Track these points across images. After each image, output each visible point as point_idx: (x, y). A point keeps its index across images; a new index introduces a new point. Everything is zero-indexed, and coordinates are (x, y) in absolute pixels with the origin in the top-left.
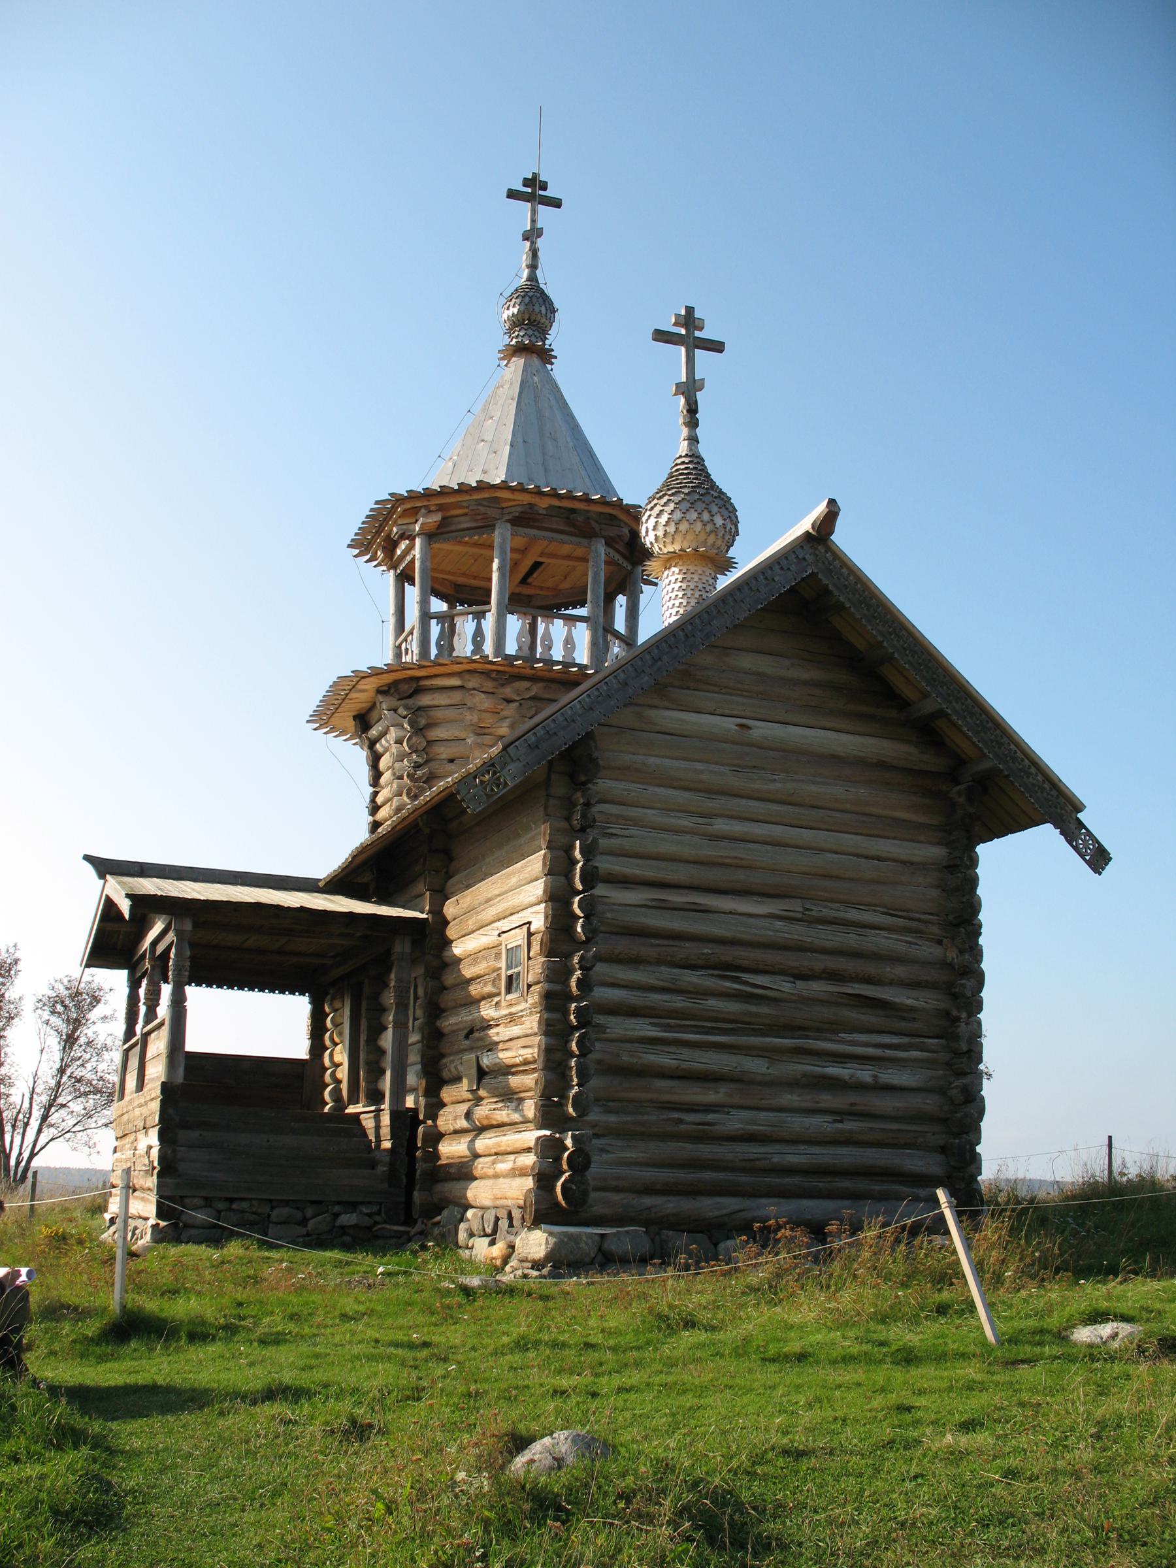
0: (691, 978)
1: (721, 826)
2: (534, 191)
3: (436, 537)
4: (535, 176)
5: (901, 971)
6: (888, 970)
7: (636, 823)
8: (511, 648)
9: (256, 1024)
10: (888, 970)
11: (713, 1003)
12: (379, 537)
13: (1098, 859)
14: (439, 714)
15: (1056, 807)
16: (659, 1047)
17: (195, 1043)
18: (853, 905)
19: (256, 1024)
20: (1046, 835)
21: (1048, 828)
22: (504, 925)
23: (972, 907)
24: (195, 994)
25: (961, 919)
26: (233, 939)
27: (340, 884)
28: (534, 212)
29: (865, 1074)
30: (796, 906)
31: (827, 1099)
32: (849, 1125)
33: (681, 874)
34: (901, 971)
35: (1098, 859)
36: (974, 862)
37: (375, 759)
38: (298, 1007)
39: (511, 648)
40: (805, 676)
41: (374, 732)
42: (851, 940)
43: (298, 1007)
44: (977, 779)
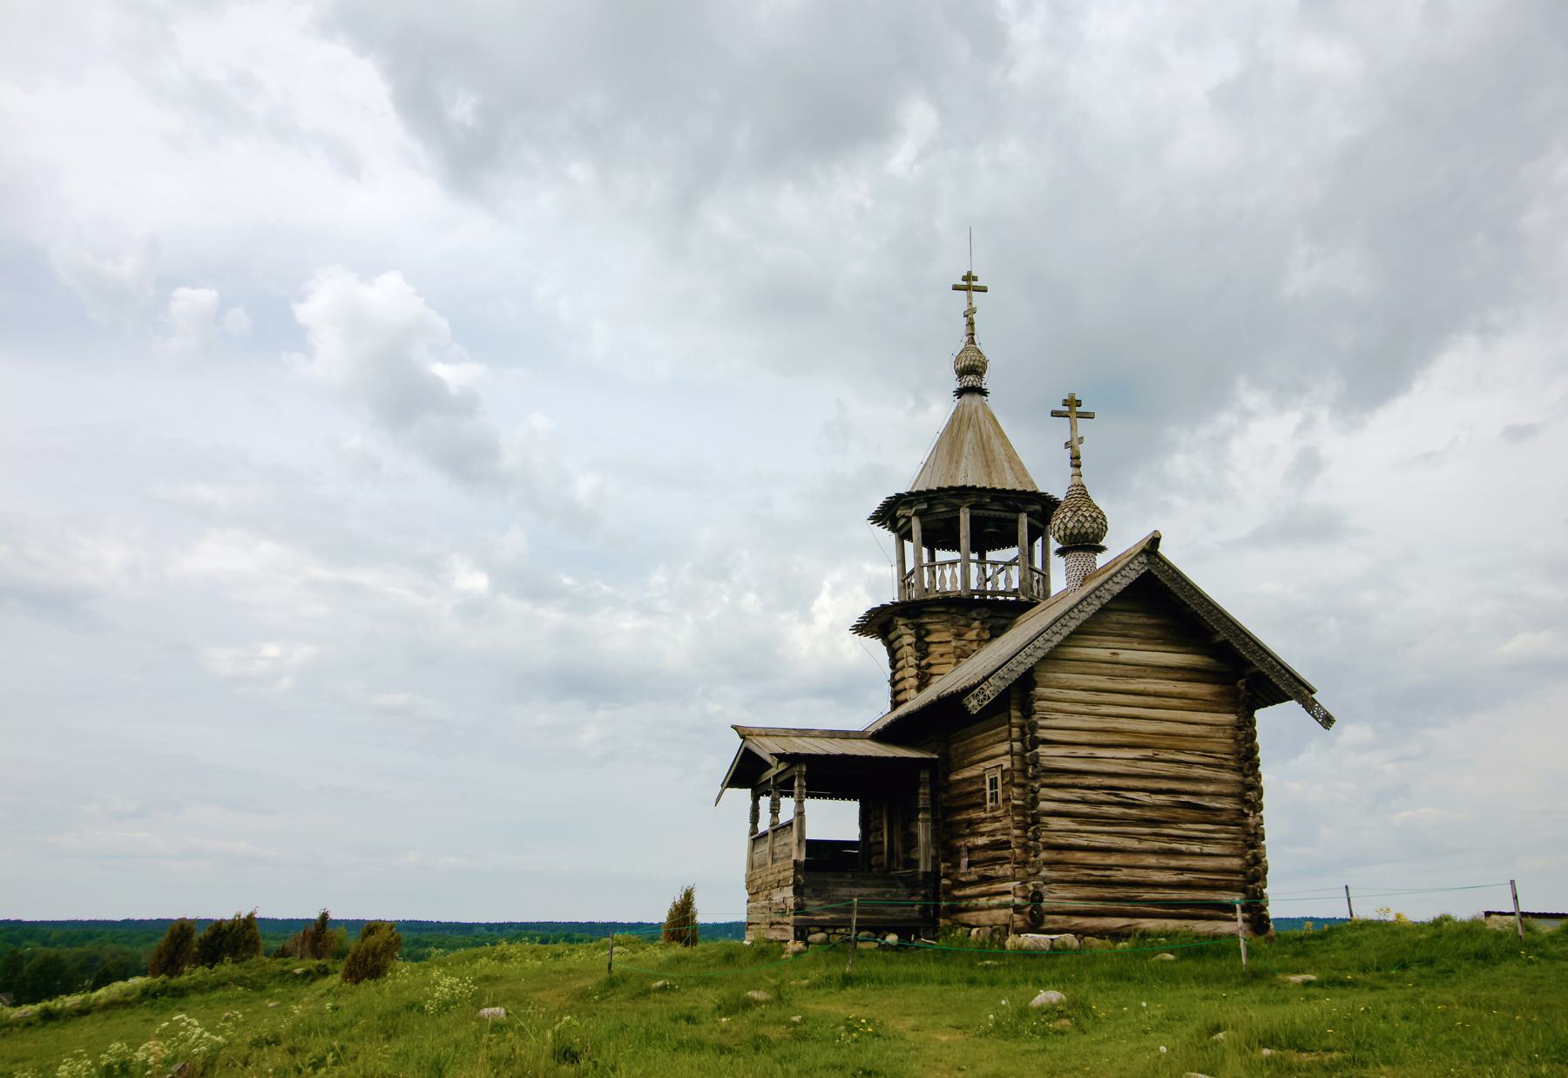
0: (1091, 795)
1: (1104, 709)
2: (969, 284)
3: (922, 516)
4: (969, 273)
5: (1211, 788)
6: (1204, 788)
7: (1057, 711)
8: (974, 585)
9: (835, 820)
10: (1204, 788)
11: (1105, 809)
12: (889, 514)
13: (1327, 721)
14: (930, 627)
15: (1299, 691)
16: (1091, 609)
17: (808, 837)
18: (1180, 750)
19: (835, 820)
20: (1293, 705)
21: (1294, 702)
22: (987, 764)
23: (1253, 750)
24: (811, 804)
25: (1247, 759)
26: (825, 774)
27: (881, 736)
28: (970, 297)
29: (1196, 848)
30: (1149, 753)
31: (1173, 863)
32: (1187, 877)
33: (1084, 737)
34: (1211, 788)
35: (1327, 721)
36: (1253, 723)
37: (893, 653)
38: (851, 808)
39: (974, 585)
40: (1141, 621)
41: (892, 636)
42: (1183, 771)
43: (851, 808)
44: (1245, 676)
